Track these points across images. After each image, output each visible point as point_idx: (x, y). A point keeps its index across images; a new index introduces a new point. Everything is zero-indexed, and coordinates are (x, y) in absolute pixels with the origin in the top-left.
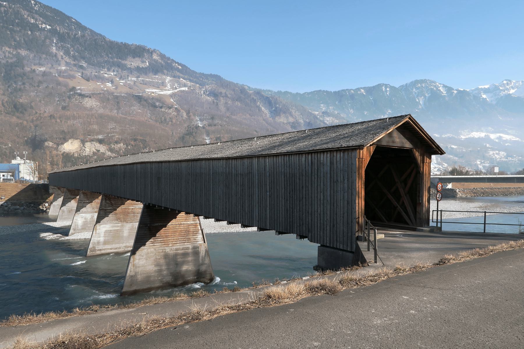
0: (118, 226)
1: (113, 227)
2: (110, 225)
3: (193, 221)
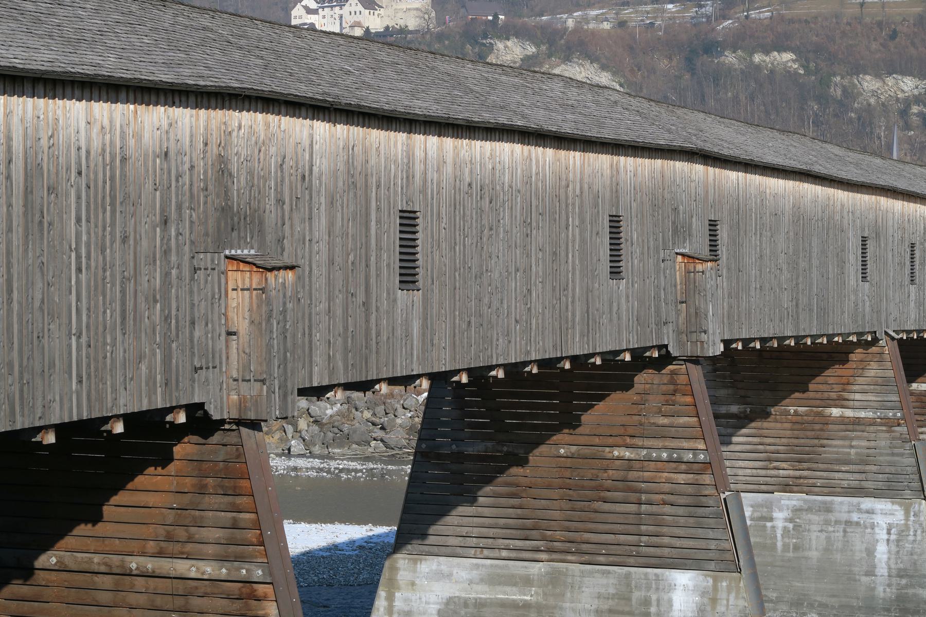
0: (527, 581)
1: (493, 580)
2: (477, 566)
3: (222, 559)
